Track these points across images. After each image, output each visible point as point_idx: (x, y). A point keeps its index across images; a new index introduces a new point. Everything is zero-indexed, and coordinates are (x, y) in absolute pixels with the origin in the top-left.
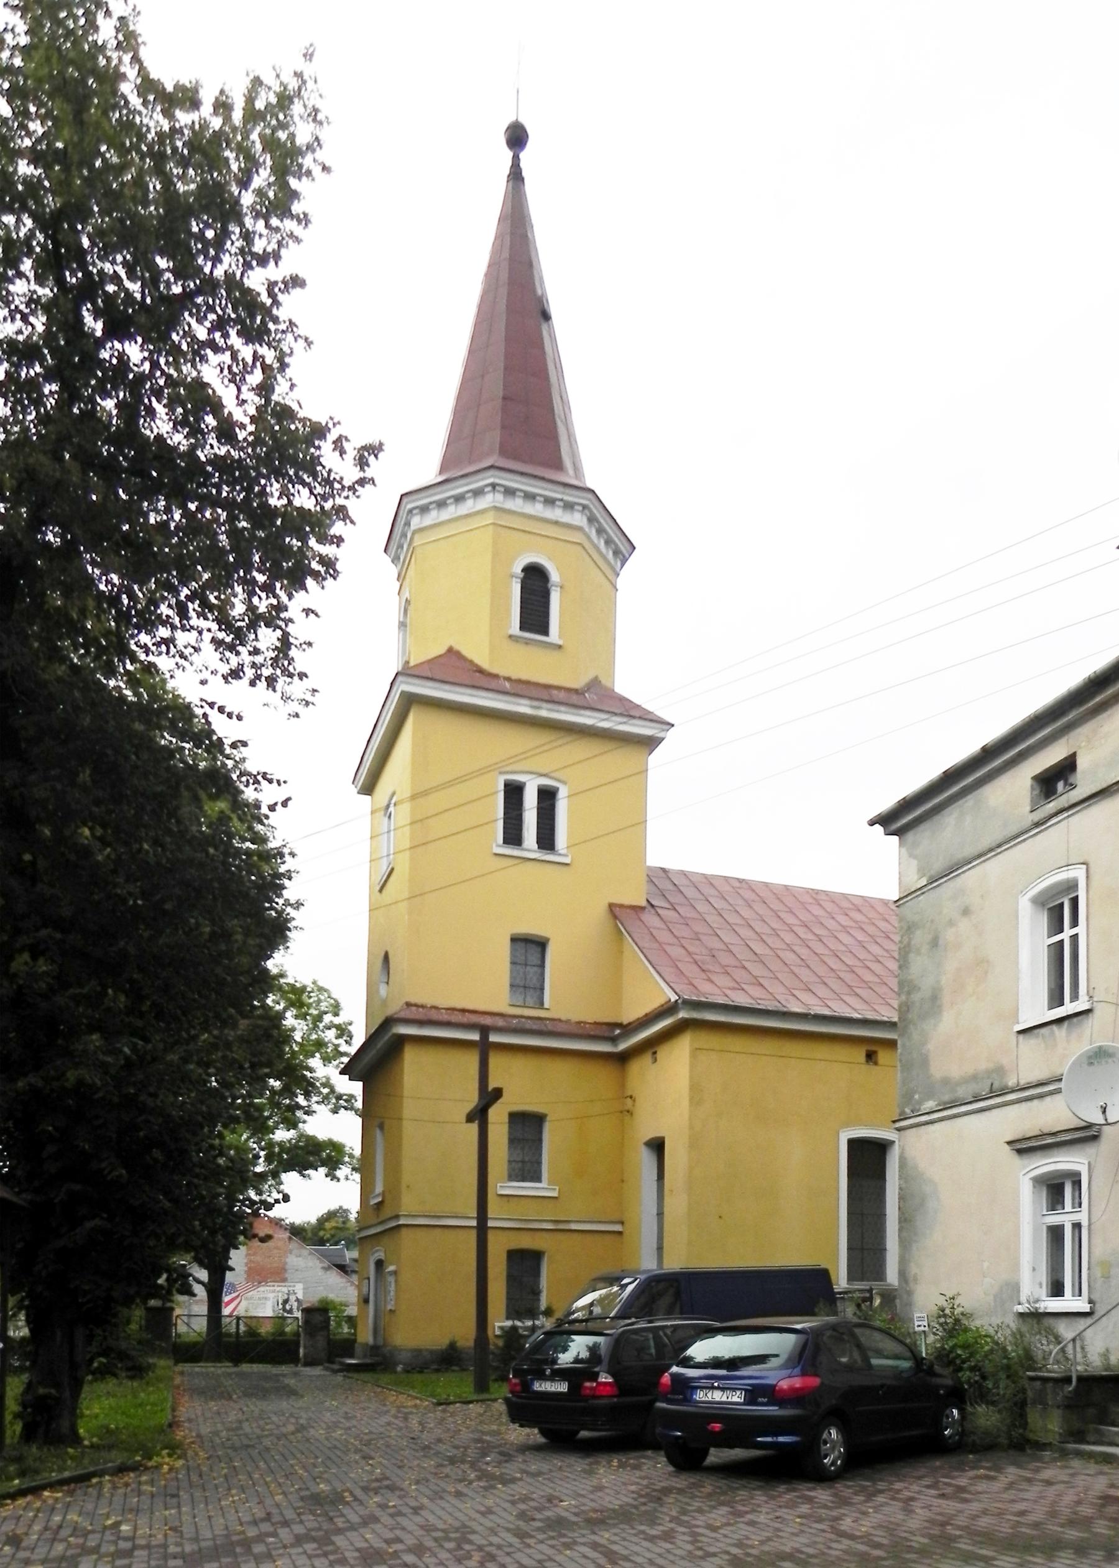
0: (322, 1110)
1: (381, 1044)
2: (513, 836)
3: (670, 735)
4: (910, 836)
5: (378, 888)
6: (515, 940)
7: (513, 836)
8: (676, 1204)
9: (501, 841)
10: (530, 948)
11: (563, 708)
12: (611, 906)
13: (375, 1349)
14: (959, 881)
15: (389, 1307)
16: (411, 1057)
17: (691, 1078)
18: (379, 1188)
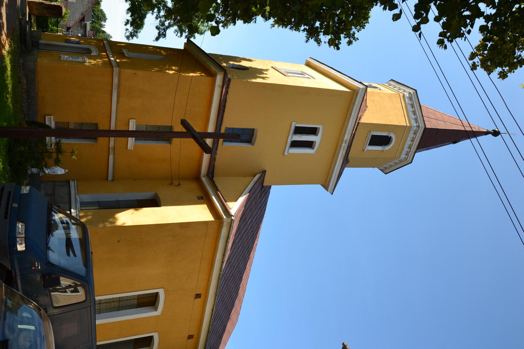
0: (157, 23)
2: (299, 131)
3: (328, 193)
6: (253, 130)
7: (299, 131)
10: (246, 136)
13: (36, 45)
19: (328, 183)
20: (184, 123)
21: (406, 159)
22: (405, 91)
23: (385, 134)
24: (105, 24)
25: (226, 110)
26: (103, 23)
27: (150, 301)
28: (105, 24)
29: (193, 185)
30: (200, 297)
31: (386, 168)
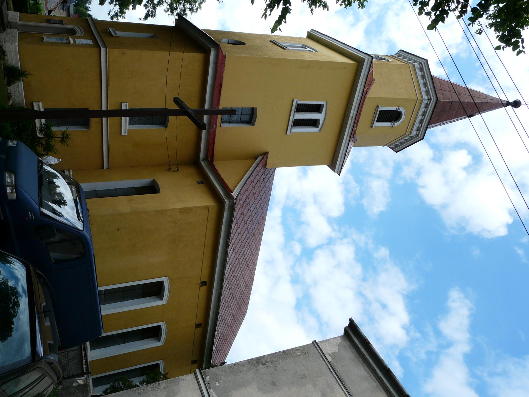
1: (207, 44)
2: (301, 108)
3: (336, 174)
4: (347, 343)
5: (272, 40)
7: (301, 108)
8: (124, 205)
9: (299, 102)
11: (351, 129)
12: (268, 153)
14: (336, 386)
15: (45, 38)
16: (198, 57)
17: (194, 207)
18: (119, 33)
19: (334, 163)
20: (177, 101)
21: (418, 135)
22: (415, 62)
23: (394, 109)
24: (90, 6)
25: (222, 92)
26: (87, 5)
27: (155, 290)
28: (90, 6)
29: (192, 171)
30: (206, 285)
31: (396, 146)
